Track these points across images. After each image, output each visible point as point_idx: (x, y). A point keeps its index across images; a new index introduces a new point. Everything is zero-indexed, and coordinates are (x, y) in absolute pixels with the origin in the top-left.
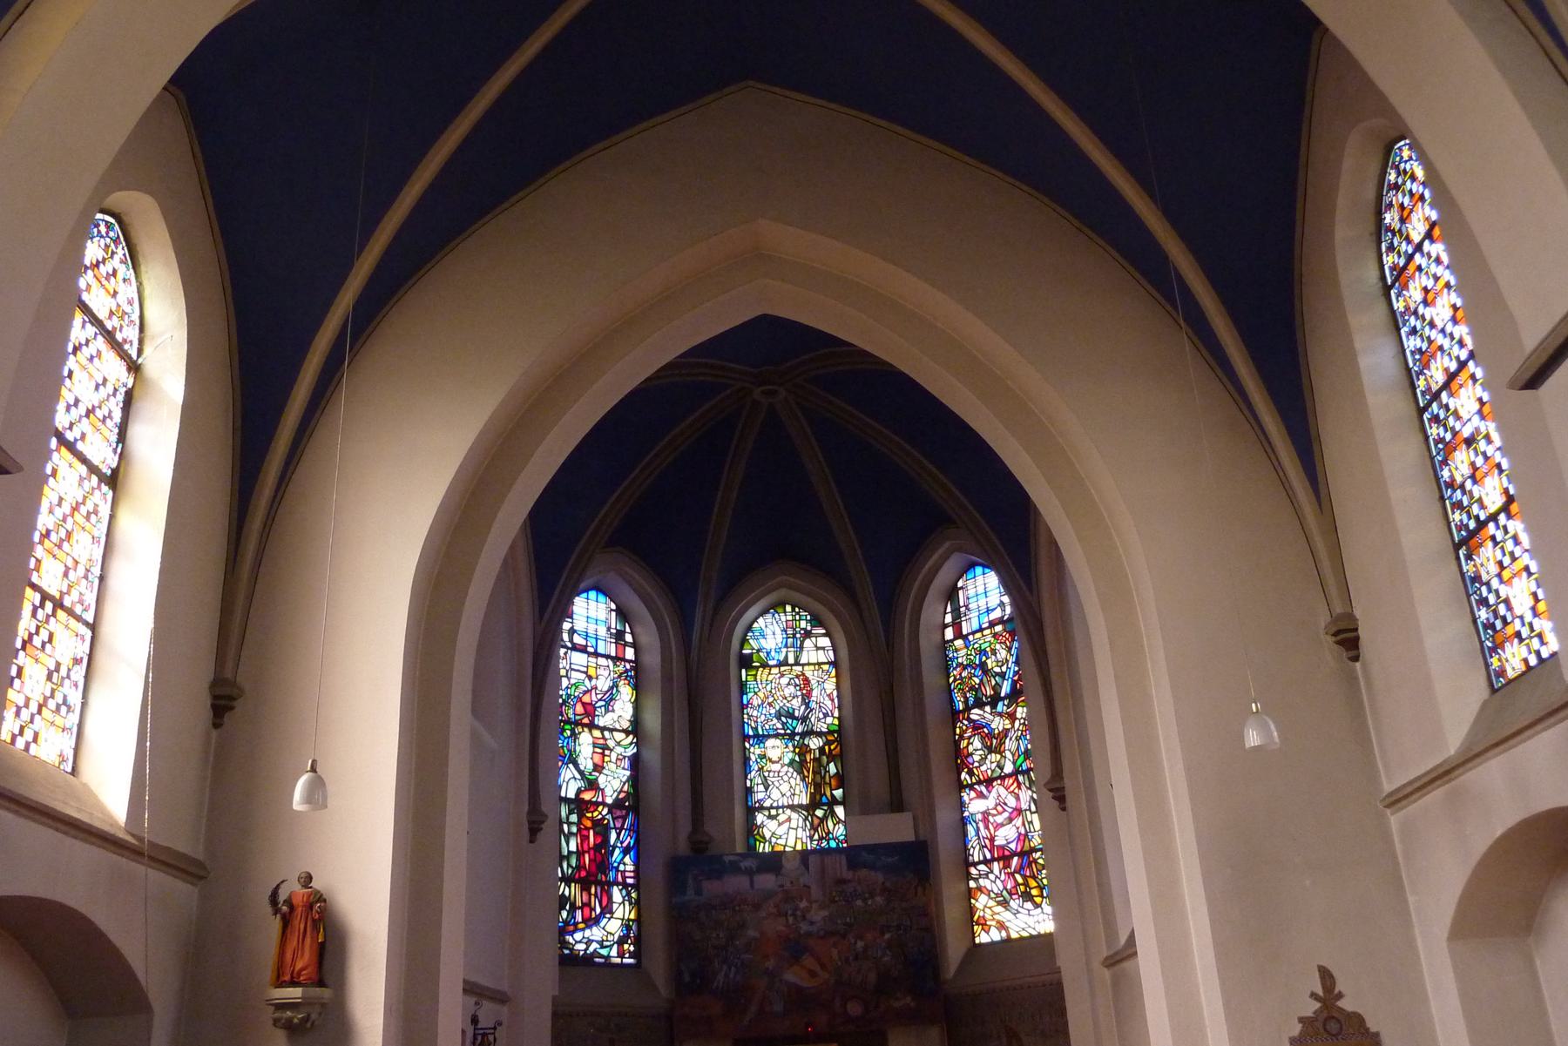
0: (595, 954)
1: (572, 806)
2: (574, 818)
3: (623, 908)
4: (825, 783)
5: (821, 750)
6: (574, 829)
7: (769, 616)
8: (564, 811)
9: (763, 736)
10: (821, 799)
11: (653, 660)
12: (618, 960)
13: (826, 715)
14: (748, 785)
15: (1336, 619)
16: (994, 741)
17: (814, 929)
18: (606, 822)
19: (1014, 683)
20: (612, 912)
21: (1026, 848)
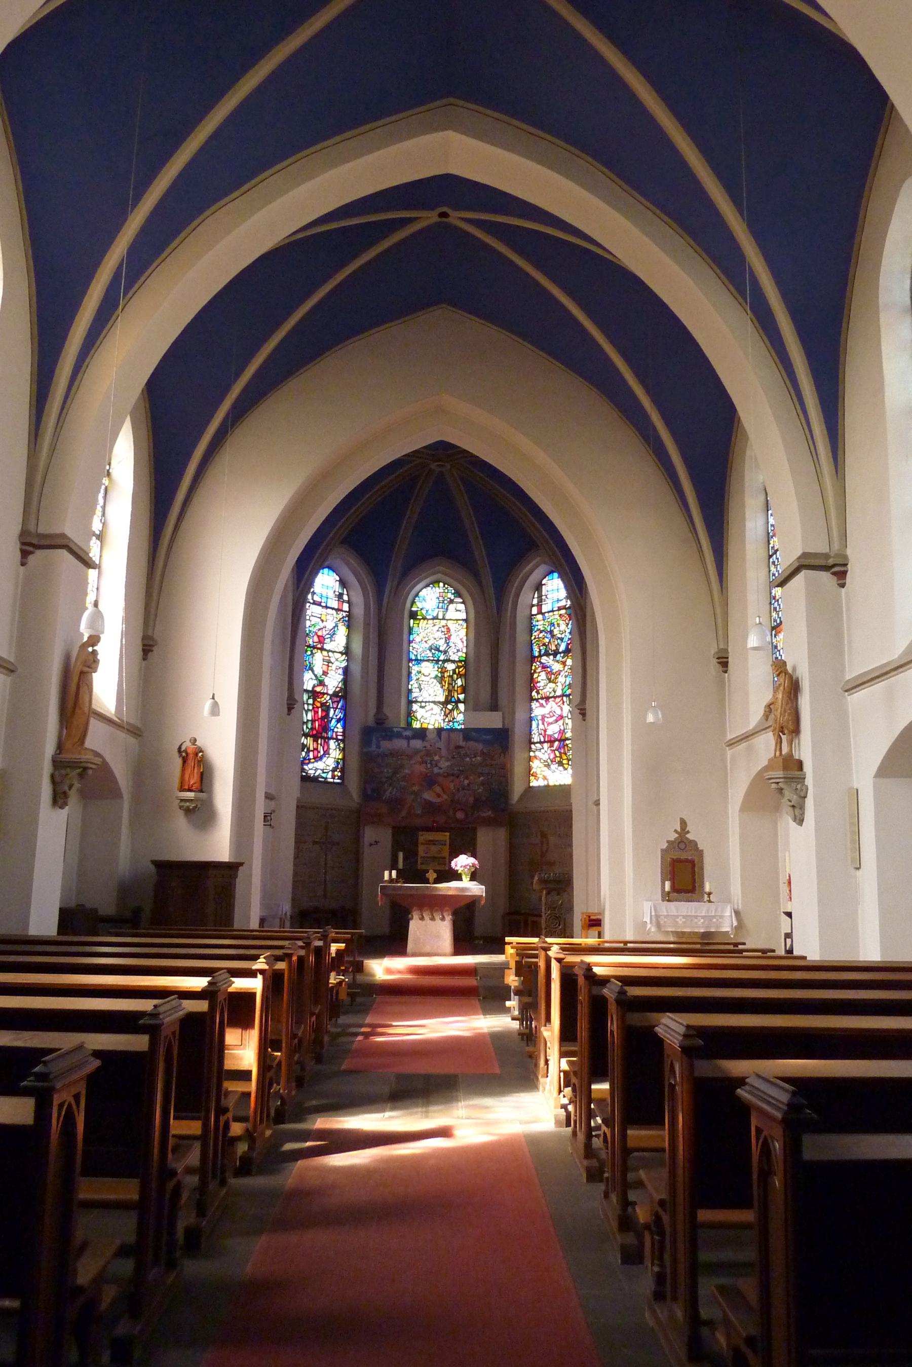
0: (319, 776)
1: (310, 695)
2: (311, 701)
3: (335, 753)
4: (454, 690)
5: (454, 671)
6: (311, 707)
7: (429, 588)
8: (305, 697)
9: (421, 660)
10: (451, 699)
11: (359, 611)
12: (332, 780)
13: (458, 651)
14: (410, 687)
15: (720, 651)
16: (553, 676)
17: (441, 771)
18: (328, 704)
19: (568, 644)
20: (329, 754)
21: (563, 738)
